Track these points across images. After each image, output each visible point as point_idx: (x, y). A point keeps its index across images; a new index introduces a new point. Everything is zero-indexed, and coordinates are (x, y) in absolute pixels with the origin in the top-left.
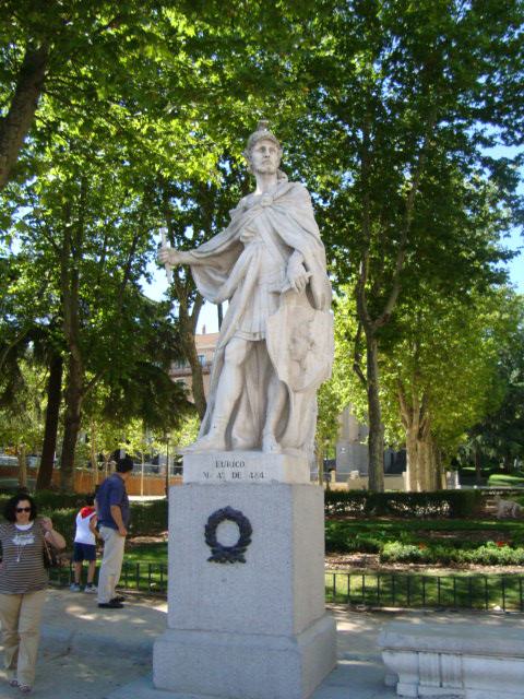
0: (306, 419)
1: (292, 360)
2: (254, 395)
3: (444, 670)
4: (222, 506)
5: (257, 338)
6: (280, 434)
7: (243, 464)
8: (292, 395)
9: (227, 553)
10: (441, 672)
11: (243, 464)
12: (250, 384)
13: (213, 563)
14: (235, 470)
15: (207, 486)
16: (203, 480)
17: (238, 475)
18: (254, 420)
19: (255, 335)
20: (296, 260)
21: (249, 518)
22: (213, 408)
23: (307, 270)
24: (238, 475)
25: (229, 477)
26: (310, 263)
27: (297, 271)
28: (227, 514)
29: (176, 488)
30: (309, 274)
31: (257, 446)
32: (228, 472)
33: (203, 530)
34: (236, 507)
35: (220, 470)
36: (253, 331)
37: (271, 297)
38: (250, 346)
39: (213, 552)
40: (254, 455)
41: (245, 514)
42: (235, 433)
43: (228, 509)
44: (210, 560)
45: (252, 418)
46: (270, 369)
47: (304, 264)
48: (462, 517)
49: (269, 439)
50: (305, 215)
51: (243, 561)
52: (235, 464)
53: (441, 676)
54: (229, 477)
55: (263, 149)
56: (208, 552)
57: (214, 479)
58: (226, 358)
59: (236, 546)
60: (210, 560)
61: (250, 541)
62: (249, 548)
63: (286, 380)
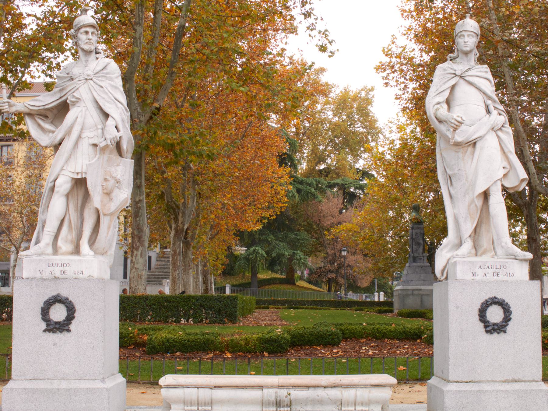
0: (110, 233)
1: (104, 193)
2: (73, 215)
3: (200, 398)
4: (54, 294)
5: (79, 177)
6: (92, 242)
7: (68, 265)
8: (102, 217)
9: (57, 326)
10: (198, 399)
11: (68, 265)
12: (71, 206)
13: (47, 333)
14: (62, 269)
16: (38, 275)
18: (74, 235)
19: (78, 173)
20: (110, 121)
21: (73, 301)
22: (43, 227)
23: (118, 130)
24: (64, 272)
25: (58, 274)
26: (120, 127)
27: (111, 133)
28: (57, 300)
29: (20, 281)
30: (118, 135)
31: (77, 251)
33: (40, 311)
34: (500, 296)
35: (51, 269)
36: (77, 172)
37: (91, 147)
38: (73, 182)
39: (48, 325)
40: (75, 258)
41: (70, 299)
42: (60, 243)
43: (58, 295)
44: (45, 331)
45: (72, 233)
46: (87, 195)
47: (116, 127)
48: (9, 271)
50: (116, 88)
51: (69, 331)
53: (198, 404)
55: (87, 33)
56: (43, 326)
58: (56, 189)
59: (64, 321)
60: (45, 331)
61: (74, 317)
62: (73, 322)
63: (99, 207)
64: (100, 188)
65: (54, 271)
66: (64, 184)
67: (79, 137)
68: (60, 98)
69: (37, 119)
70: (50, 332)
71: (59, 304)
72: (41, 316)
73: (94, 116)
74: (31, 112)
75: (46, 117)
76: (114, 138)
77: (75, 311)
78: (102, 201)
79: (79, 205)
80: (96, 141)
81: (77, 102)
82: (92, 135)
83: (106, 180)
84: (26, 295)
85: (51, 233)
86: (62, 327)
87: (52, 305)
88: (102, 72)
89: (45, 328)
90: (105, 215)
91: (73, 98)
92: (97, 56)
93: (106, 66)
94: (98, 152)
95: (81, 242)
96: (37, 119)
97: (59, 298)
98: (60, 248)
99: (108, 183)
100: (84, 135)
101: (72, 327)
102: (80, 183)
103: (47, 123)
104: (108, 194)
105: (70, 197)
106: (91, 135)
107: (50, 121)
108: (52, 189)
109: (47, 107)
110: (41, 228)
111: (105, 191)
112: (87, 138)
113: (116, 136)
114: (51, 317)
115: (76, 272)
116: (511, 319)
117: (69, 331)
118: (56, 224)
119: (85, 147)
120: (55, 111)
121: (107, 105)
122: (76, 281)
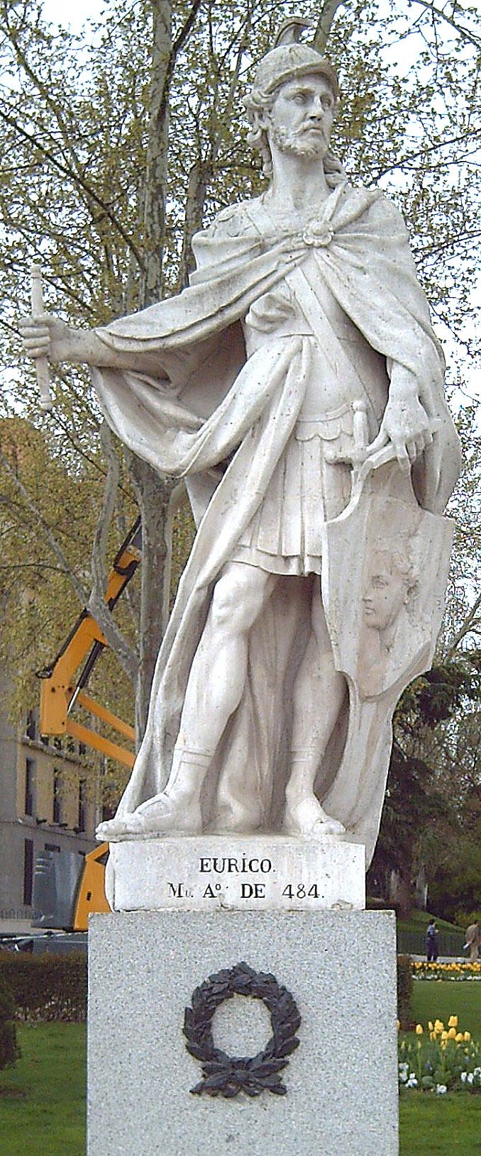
5: (293, 570)
6: (322, 791)
7: (267, 866)
9: (240, 1073)
11: (267, 866)
13: (206, 1100)
14: (250, 878)
15: (183, 916)
17: (255, 891)
19: (287, 559)
24: (255, 891)
25: (232, 896)
28: (239, 982)
29: (108, 919)
31: (273, 819)
32: (231, 885)
35: (210, 878)
37: (328, 472)
39: (207, 1071)
41: (282, 981)
43: (242, 968)
44: (197, 1091)
49: (247, 868)
51: (279, 1090)
52: (248, 866)
54: (232, 896)
56: (193, 1072)
57: (196, 900)
60: (197, 1091)
63: (350, 670)
64: (356, 606)
65: (218, 887)
66: (238, 594)
67: (294, 438)
68: (221, 310)
69: (134, 385)
70: (214, 1096)
71: (243, 999)
72: (183, 1040)
73: (337, 373)
74: (120, 362)
75: (164, 379)
76: (418, 436)
77: (297, 1024)
78: (361, 654)
79: (281, 667)
80: (350, 451)
81: (283, 320)
82: (339, 430)
83: (376, 580)
84: (133, 967)
85: (194, 758)
86: (228, 1079)
87: (219, 1002)
88: (355, 226)
89: (200, 1080)
90: (365, 699)
91: (269, 307)
92: (331, 178)
93: (367, 208)
94: (357, 489)
95: (290, 791)
96: (134, 385)
97: (244, 979)
98: (227, 808)
99: (383, 592)
100: (307, 432)
101: (292, 1076)
102: (295, 593)
103: (168, 399)
104: (380, 628)
105: (255, 640)
106: (330, 431)
107: (175, 393)
108: (202, 614)
109: (172, 342)
110: (158, 744)
111: (373, 620)
112: (317, 441)
113: (425, 431)
114: (218, 1044)
115: (294, 891)
116: (297, 1043)
117: (279, 1090)
118: (215, 729)
119: (312, 473)
120: (192, 360)
121: (384, 328)
122: (301, 918)
